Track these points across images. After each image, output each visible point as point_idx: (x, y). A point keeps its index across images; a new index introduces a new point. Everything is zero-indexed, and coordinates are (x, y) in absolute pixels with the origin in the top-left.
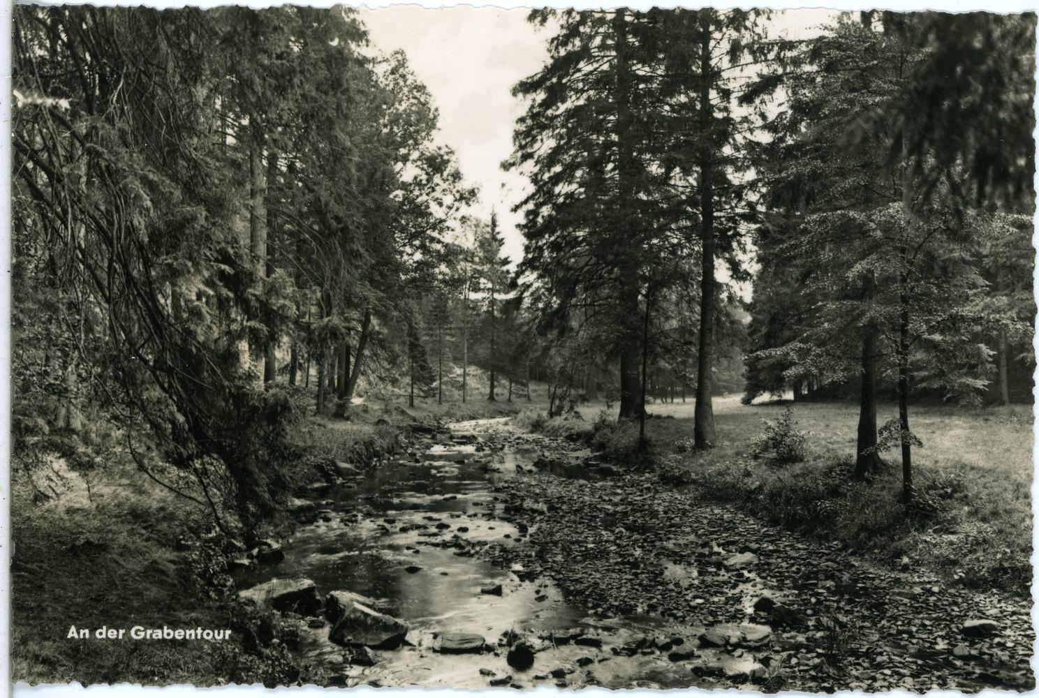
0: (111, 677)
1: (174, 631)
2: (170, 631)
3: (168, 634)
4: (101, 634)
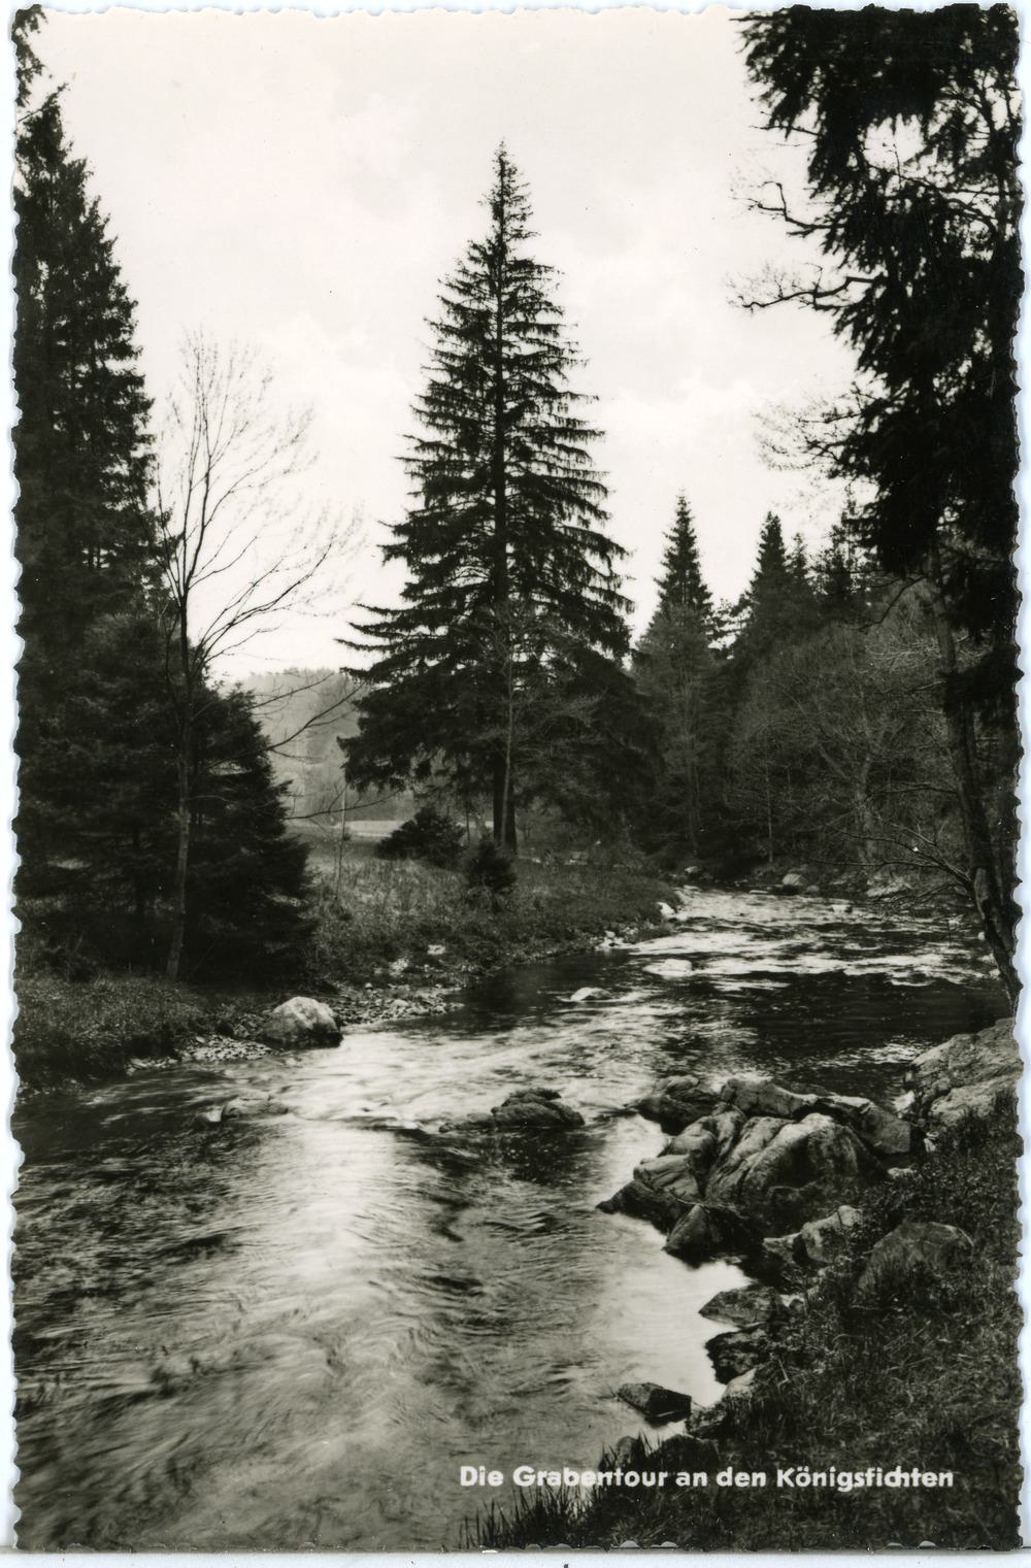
1: (580, 1474)
2: (575, 1474)
3: (571, 1479)
4: (725, 1479)
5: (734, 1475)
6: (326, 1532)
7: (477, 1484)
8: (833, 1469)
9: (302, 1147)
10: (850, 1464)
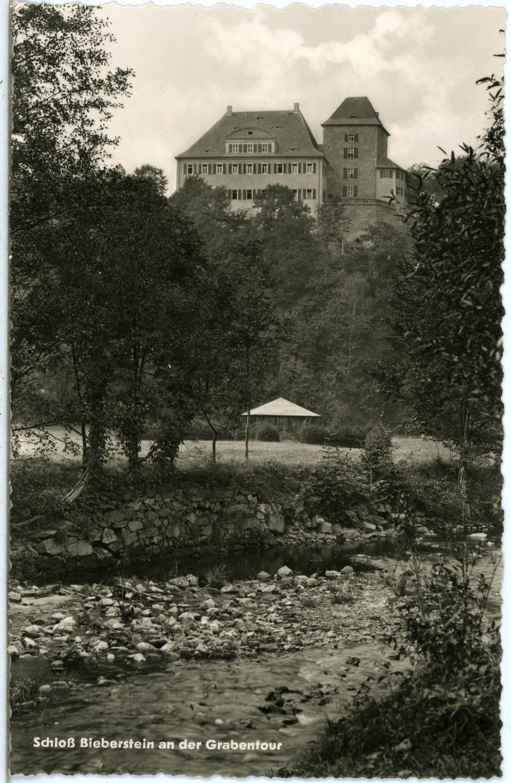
2: (236, 744)
3: (234, 746)
4: (183, 746)
5: (188, 743)
8: (91, 739)
10: (63, 733)
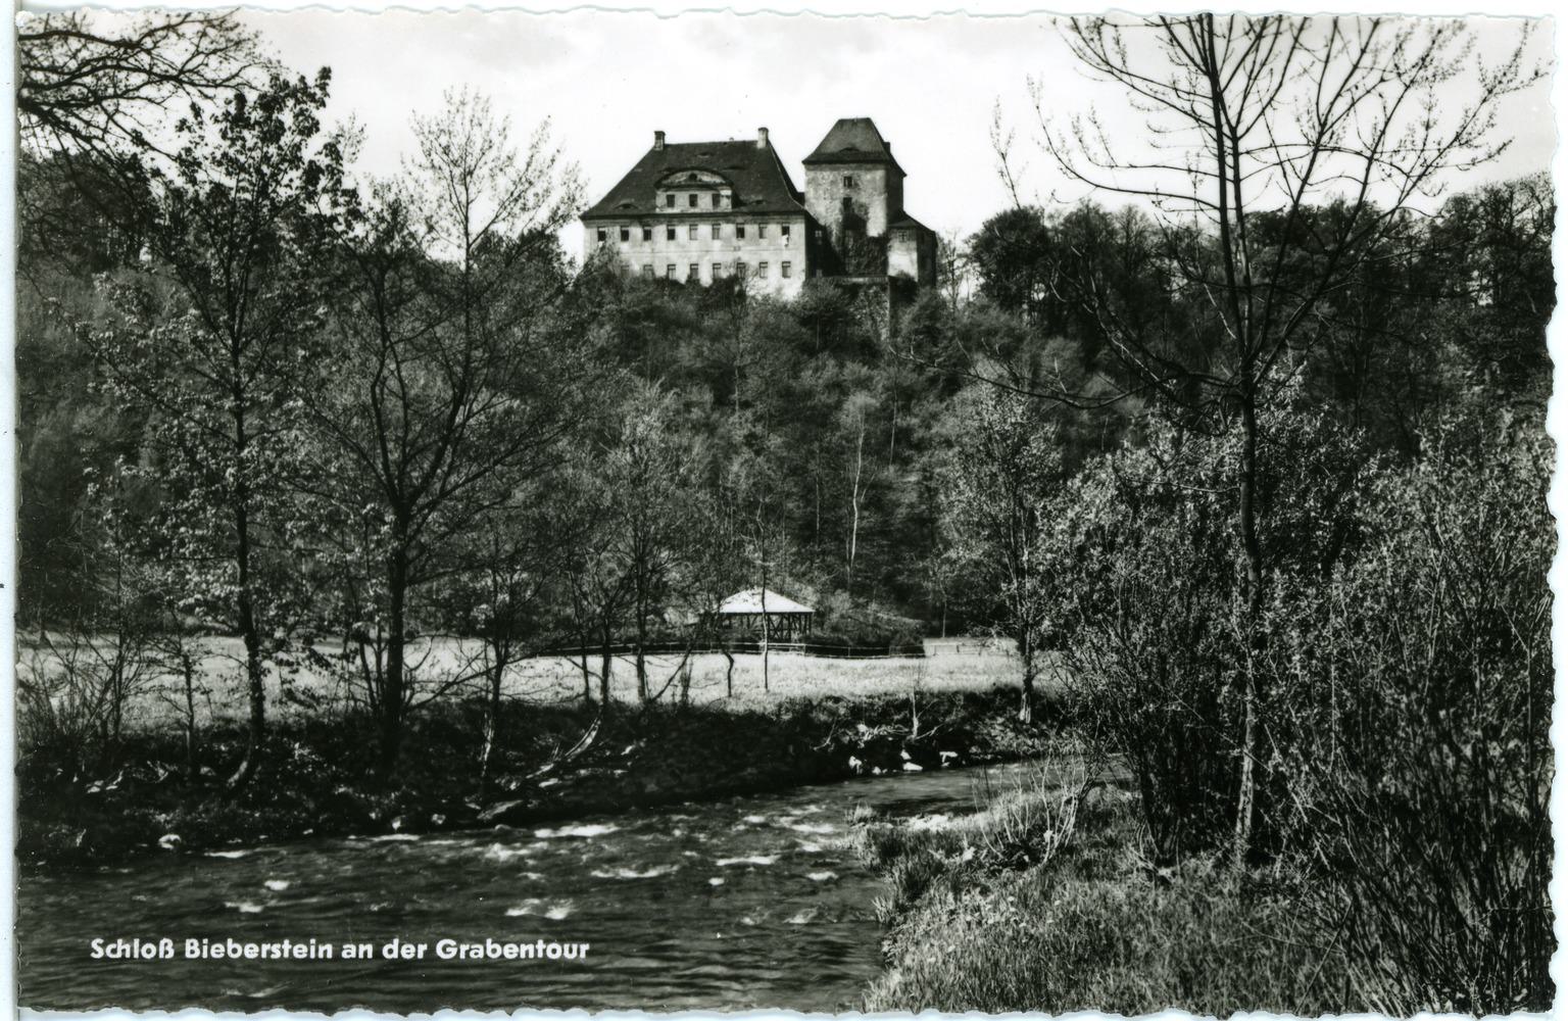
0: (173, 1004)
2: (238, 946)
3: (494, 951)
4: (390, 951)
6: (25, 259)
7: (200, 957)
9: (1306, 19)
